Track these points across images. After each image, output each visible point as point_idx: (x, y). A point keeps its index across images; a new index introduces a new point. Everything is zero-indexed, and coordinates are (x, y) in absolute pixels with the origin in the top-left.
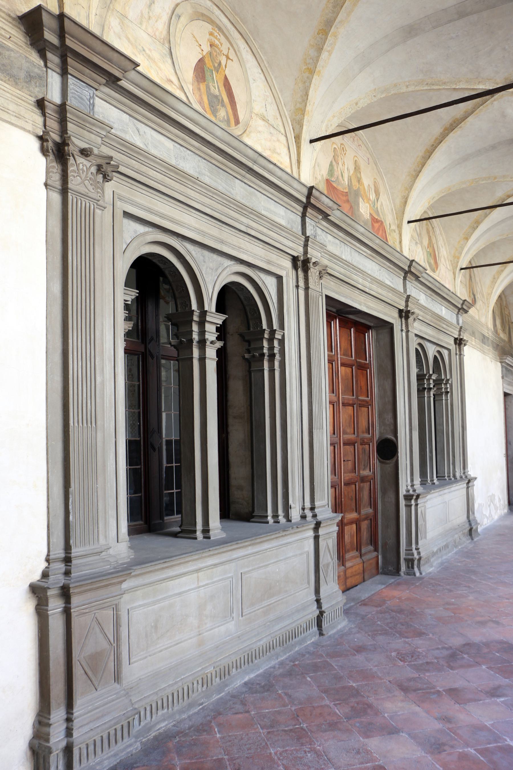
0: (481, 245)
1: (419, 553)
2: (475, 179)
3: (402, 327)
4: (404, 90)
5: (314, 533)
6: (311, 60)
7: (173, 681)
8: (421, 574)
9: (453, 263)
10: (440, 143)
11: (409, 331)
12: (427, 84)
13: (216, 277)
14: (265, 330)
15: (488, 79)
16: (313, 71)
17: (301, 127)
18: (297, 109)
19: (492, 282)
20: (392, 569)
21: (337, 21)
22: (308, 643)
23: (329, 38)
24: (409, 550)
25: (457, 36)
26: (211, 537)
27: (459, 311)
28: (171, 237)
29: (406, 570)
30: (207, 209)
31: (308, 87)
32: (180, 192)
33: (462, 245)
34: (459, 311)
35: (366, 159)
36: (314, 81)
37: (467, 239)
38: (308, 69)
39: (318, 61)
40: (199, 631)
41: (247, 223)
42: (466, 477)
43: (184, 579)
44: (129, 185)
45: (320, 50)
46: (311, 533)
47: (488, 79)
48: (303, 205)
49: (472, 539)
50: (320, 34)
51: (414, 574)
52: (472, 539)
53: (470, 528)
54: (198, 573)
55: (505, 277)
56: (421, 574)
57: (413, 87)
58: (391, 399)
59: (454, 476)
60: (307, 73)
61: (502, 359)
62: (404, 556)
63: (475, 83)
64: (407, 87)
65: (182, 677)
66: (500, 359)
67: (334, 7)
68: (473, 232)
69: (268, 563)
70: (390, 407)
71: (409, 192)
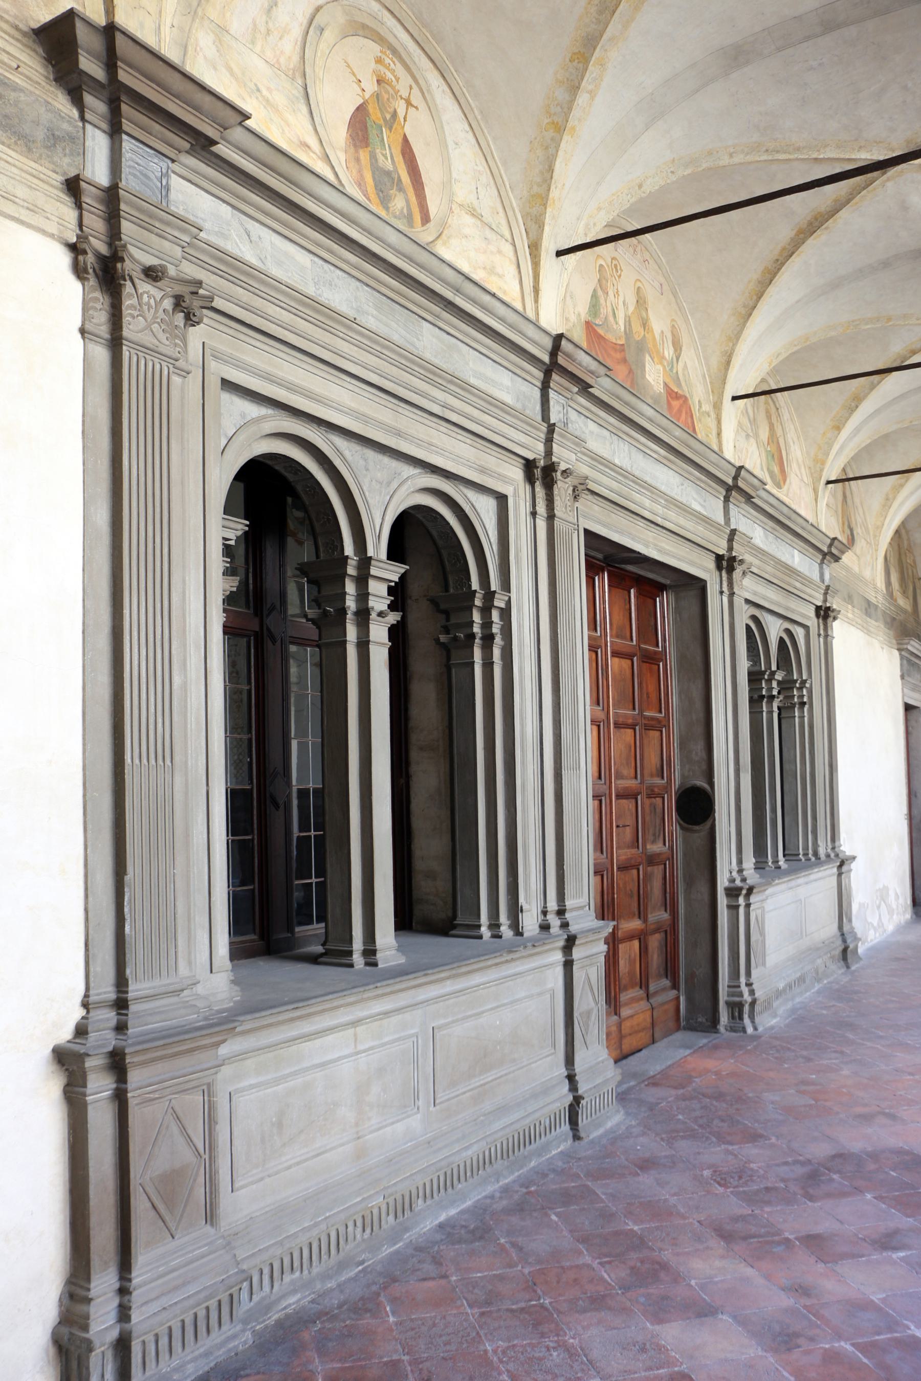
0: (863, 439)
1: (752, 992)
2: (853, 321)
3: (721, 587)
4: (725, 161)
5: (563, 957)
6: (559, 107)
7: (311, 1221)
8: (755, 1029)
9: (813, 471)
10: (791, 256)
11: (734, 593)
12: (767, 150)
13: (388, 498)
14: (475, 591)
15: (876, 142)
16: (562, 128)
17: (541, 227)
18: (533, 196)
19: (884, 506)
20: (704, 1020)
21: (605, 37)
22: (553, 1153)
23: (590, 67)
24: (734, 986)
25: (820, 64)
26: (379, 963)
27: (824, 558)
28: (307, 426)
29: (729, 1023)
30: (372, 374)
31: (552, 155)
32: (323, 344)
33: (830, 439)
34: (824, 558)
35: (657, 285)
36: (563, 145)
37: (838, 429)
38: (553, 123)
39: (570, 109)
40: (357, 1133)
41: (443, 400)
42: (837, 855)
43: (330, 1039)
44: (231, 332)
45: (574, 89)
46: (559, 957)
47: (876, 142)
48: (545, 367)
49: (848, 967)
50: (574, 60)
51: (744, 1030)
52: (848, 967)
53: (843, 947)
54: (355, 1027)
55: (907, 498)
56: (755, 1029)
57: (742, 156)
58: (701, 715)
59: (816, 854)
60: (552, 131)
61: (902, 644)
62: (726, 998)
63: (854, 149)
64: (731, 155)
65: (327, 1215)
66: (898, 644)
67: (600, 12)
68: (850, 417)
69: (481, 1009)
70: (700, 730)
71: (735, 345)
